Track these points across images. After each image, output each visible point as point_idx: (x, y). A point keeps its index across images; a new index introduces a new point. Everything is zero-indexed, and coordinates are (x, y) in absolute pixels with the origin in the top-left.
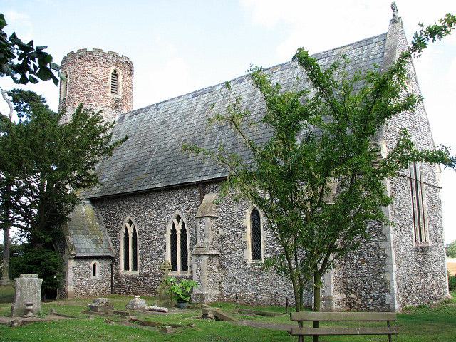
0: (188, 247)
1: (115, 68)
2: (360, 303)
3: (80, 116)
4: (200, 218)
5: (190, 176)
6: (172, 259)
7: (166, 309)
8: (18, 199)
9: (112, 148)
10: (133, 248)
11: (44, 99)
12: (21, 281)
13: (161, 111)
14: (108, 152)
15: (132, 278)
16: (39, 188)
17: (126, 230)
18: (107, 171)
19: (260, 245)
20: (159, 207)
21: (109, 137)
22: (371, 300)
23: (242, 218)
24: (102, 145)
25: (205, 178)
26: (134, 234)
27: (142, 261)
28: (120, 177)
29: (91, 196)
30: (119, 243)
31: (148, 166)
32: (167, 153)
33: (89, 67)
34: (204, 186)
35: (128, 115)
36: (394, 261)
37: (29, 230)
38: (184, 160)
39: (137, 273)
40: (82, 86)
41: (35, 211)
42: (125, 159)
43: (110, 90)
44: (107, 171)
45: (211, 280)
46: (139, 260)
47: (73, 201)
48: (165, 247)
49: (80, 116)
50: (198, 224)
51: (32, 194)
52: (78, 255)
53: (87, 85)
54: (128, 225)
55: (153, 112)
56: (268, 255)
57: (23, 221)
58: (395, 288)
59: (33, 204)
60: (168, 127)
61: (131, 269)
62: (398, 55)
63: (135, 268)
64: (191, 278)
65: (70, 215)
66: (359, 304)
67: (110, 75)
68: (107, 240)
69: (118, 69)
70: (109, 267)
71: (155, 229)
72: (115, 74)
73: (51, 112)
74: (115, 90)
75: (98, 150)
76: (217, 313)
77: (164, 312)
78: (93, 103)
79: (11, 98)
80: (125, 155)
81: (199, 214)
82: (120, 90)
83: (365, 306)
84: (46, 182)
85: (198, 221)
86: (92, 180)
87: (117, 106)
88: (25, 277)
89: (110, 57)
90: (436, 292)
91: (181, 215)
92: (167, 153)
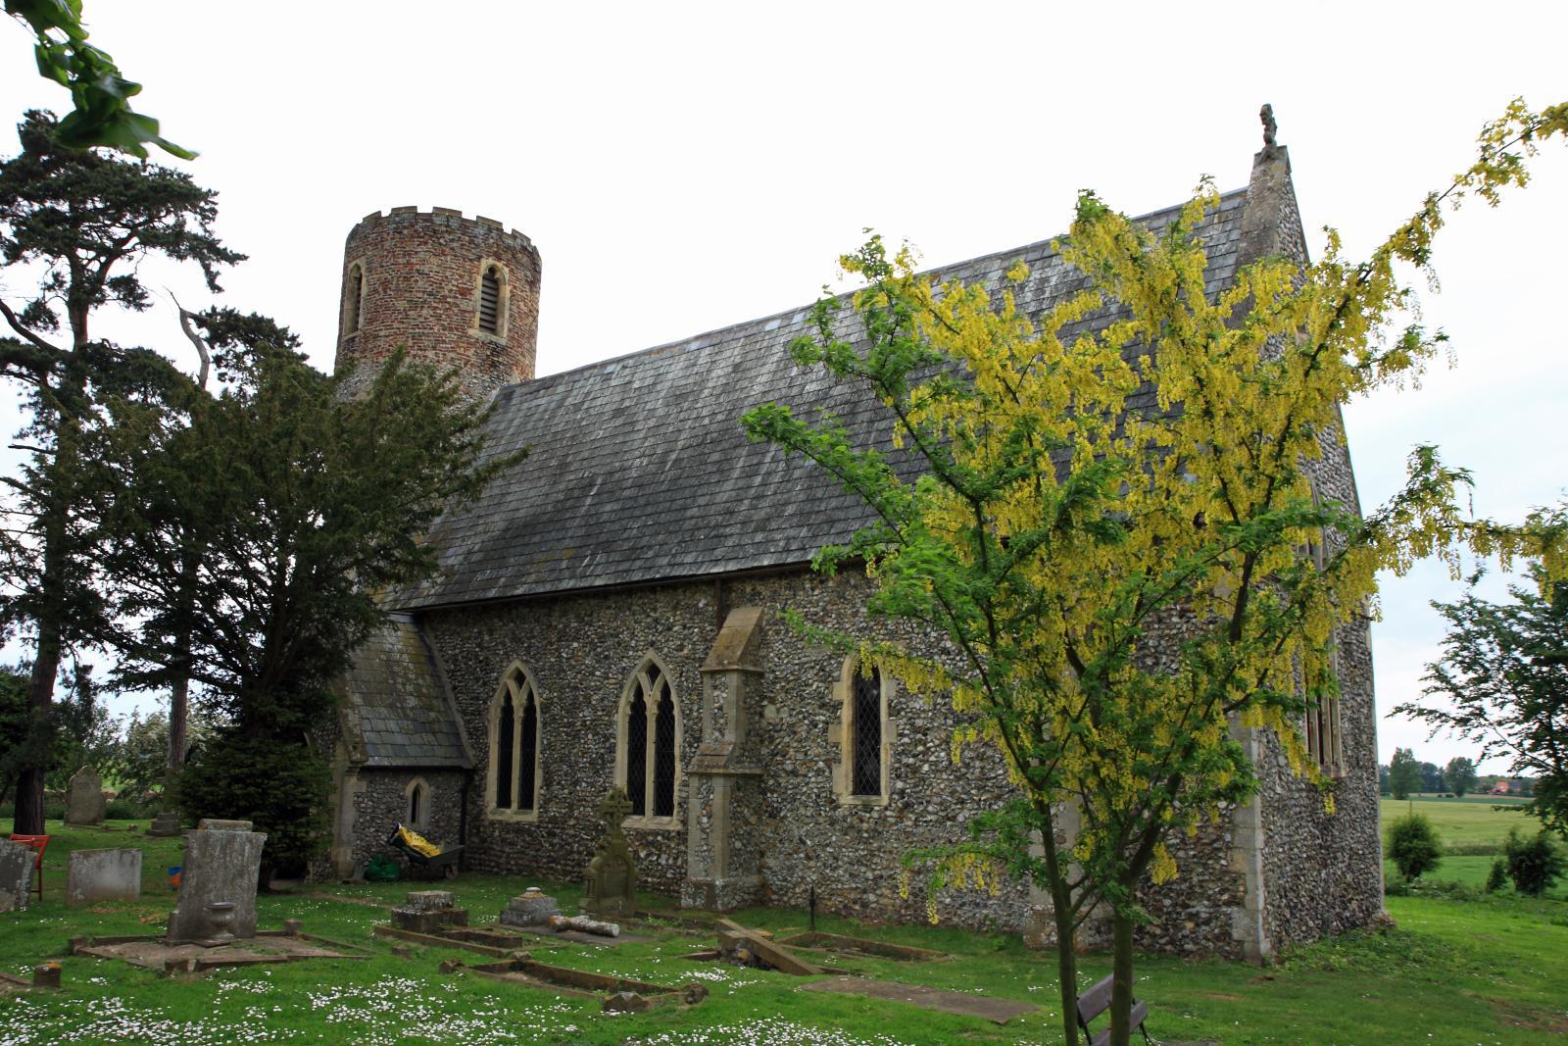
0: (677, 751)
1: (491, 261)
2: (1158, 931)
3: (396, 388)
4: (713, 673)
5: (689, 559)
6: (631, 782)
7: (615, 928)
8: (210, 603)
9: (483, 479)
10: (512, 721)
11: (293, 339)
12: (206, 839)
13: (613, 383)
14: (470, 488)
15: (518, 829)
16: (271, 577)
17: (508, 698)
18: (459, 542)
19: (877, 756)
20: (602, 638)
21: (477, 448)
22: (1190, 925)
23: (829, 679)
24: (454, 468)
25: (732, 567)
26: (530, 709)
27: (548, 783)
28: (496, 553)
29: (413, 604)
30: (485, 733)
31: (575, 527)
32: (626, 493)
33: (422, 255)
34: (726, 589)
35: (525, 390)
36: (1258, 820)
37: (236, 689)
38: (672, 516)
39: (532, 816)
40: (401, 305)
41: (257, 640)
42: (512, 506)
43: (477, 322)
44: (459, 542)
45: (738, 845)
46: (538, 781)
47: (369, 617)
48: (612, 750)
49: (396, 388)
50: (707, 691)
51: (251, 590)
52: (371, 762)
53: (415, 305)
54: (512, 685)
55: (592, 384)
56: (900, 785)
57: (220, 665)
58: (1261, 894)
59: (251, 620)
60: (632, 423)
61: (515, 805)
62: (483, 459)
63: (526, 803)
64: (682, 836)
65: (356, 655)
66: (1154, 936)
67: (480, 281)
68: (453, 723)
69: (500, 265)
70: (457, 796)
71: (588, 698)
72: (492, 279)
73: (312, 373)
74: (490, 323)
75: (443, 482)
76: (761, 947)
77: (609, 935)
78: (430, 354)
79: (204, 333)
80: (520, 496)
81: (711, 663)
82: (505, 324)
83: (1171, 942)
84: (292, 560)
85: (707, 680)
86: (420, 564)
87: (494, 365)
88: (215, 828)
89: (481, 231)
90: (1354, 905)
91: (661, 665)
92: (626, 493)
